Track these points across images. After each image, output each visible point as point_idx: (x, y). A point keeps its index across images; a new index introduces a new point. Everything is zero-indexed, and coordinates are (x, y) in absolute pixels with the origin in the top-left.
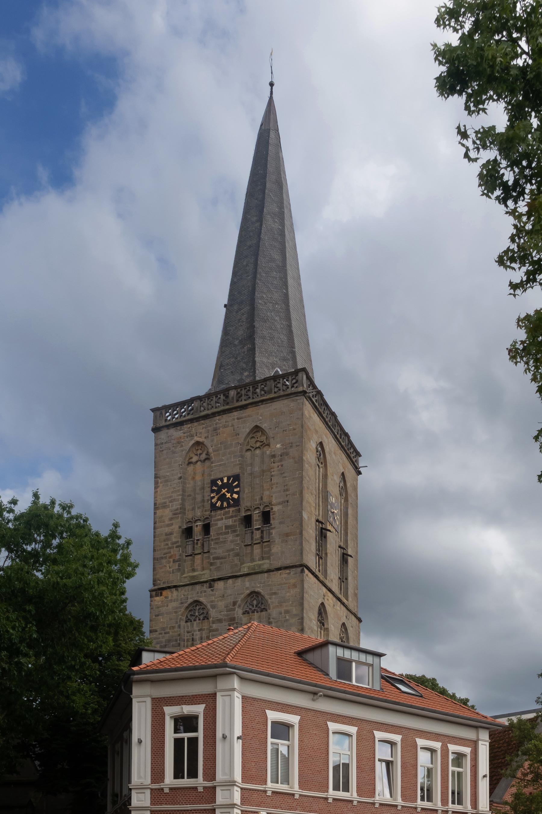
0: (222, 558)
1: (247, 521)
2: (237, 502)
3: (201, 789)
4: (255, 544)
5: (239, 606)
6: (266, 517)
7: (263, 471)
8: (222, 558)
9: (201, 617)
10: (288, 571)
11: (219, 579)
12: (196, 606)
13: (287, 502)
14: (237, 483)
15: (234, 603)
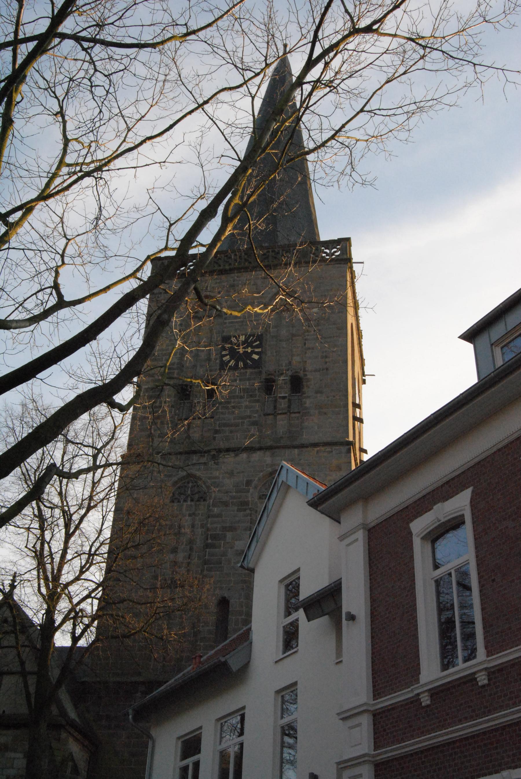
0: (231, 425)
1: (269, 386)
2: (257, 364)
3: (482, 679)
4: (278, 414)
5: (256, 487)
6: (297, 383)
7: (293, 335)
8: (231, 425)
9: (196, 497)
10: (328, 449)
11: (228, 450)
12: (188, 483)
13: (327, 369)
14: (258, 342)
15: (249, 483)
